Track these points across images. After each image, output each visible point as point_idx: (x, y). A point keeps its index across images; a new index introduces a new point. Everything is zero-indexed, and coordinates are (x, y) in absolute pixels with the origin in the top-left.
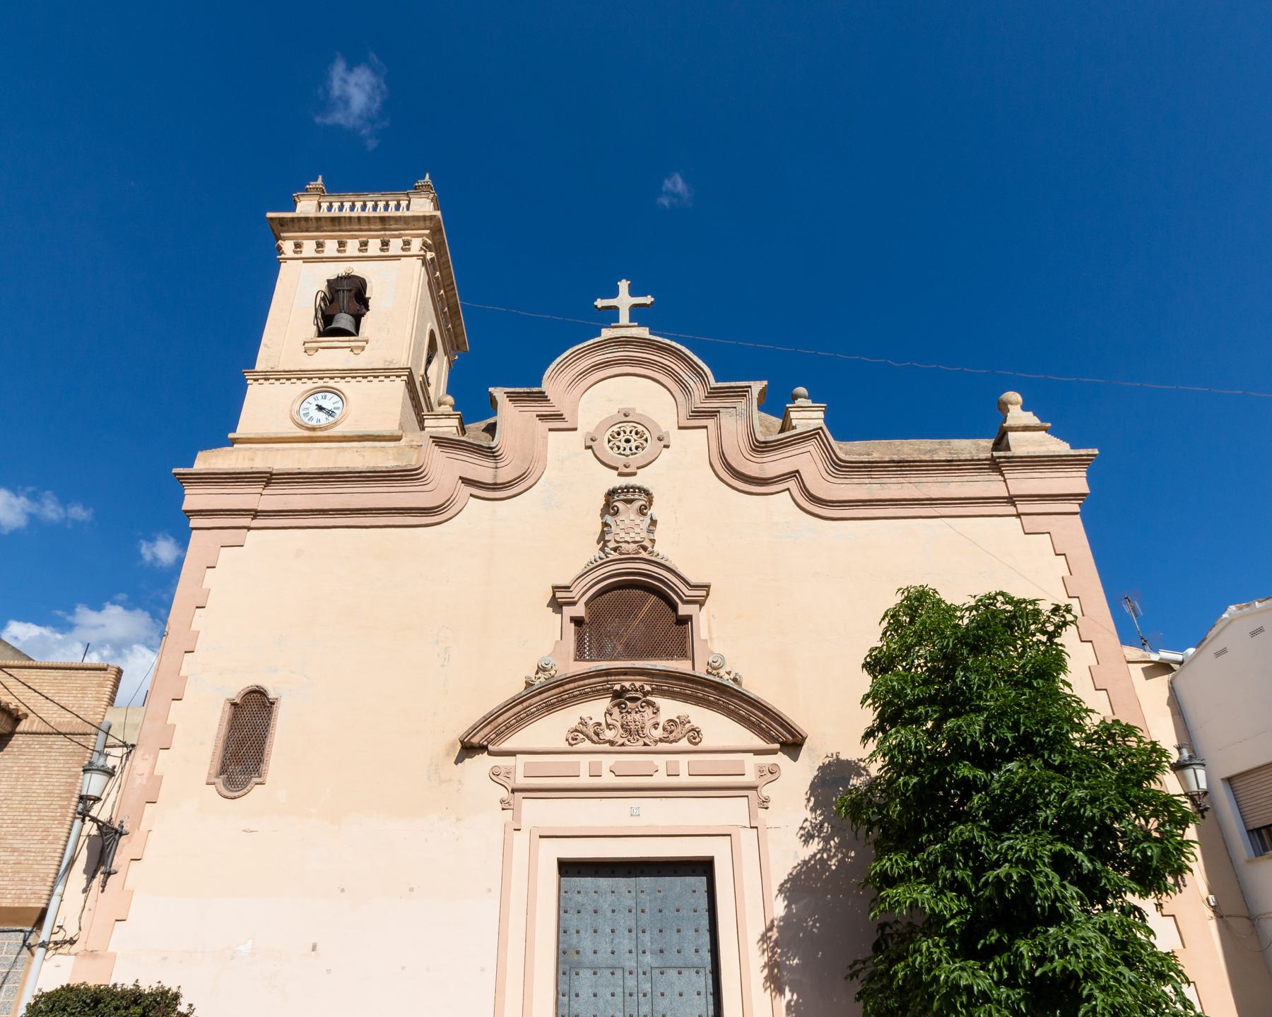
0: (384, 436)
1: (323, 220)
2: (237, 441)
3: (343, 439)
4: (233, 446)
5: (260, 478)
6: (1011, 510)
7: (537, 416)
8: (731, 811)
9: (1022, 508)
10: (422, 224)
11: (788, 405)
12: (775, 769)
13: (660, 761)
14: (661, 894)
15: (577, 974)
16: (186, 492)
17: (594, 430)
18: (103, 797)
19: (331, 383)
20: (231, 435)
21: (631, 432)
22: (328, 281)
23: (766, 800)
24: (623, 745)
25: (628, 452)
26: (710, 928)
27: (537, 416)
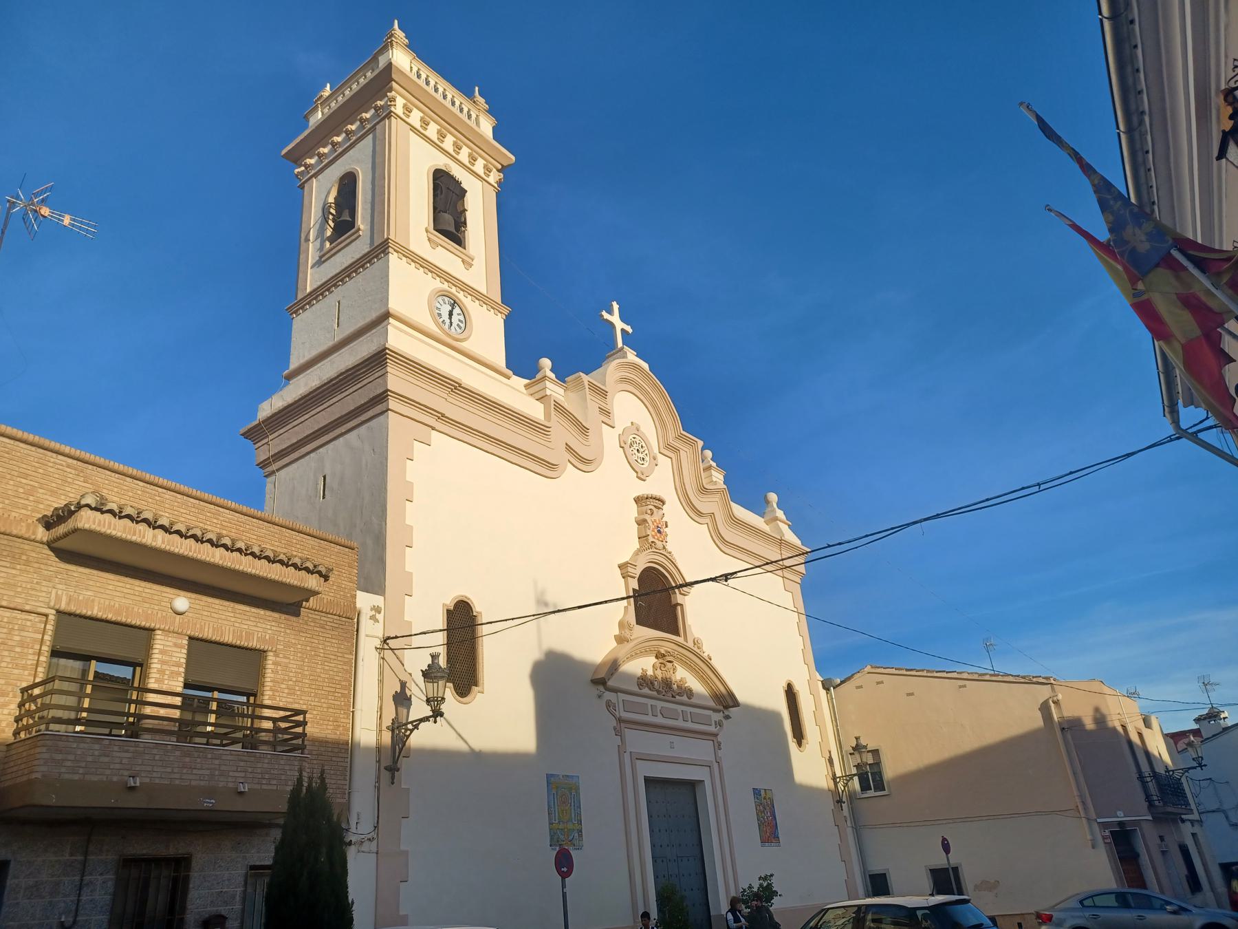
7: (599, 408)
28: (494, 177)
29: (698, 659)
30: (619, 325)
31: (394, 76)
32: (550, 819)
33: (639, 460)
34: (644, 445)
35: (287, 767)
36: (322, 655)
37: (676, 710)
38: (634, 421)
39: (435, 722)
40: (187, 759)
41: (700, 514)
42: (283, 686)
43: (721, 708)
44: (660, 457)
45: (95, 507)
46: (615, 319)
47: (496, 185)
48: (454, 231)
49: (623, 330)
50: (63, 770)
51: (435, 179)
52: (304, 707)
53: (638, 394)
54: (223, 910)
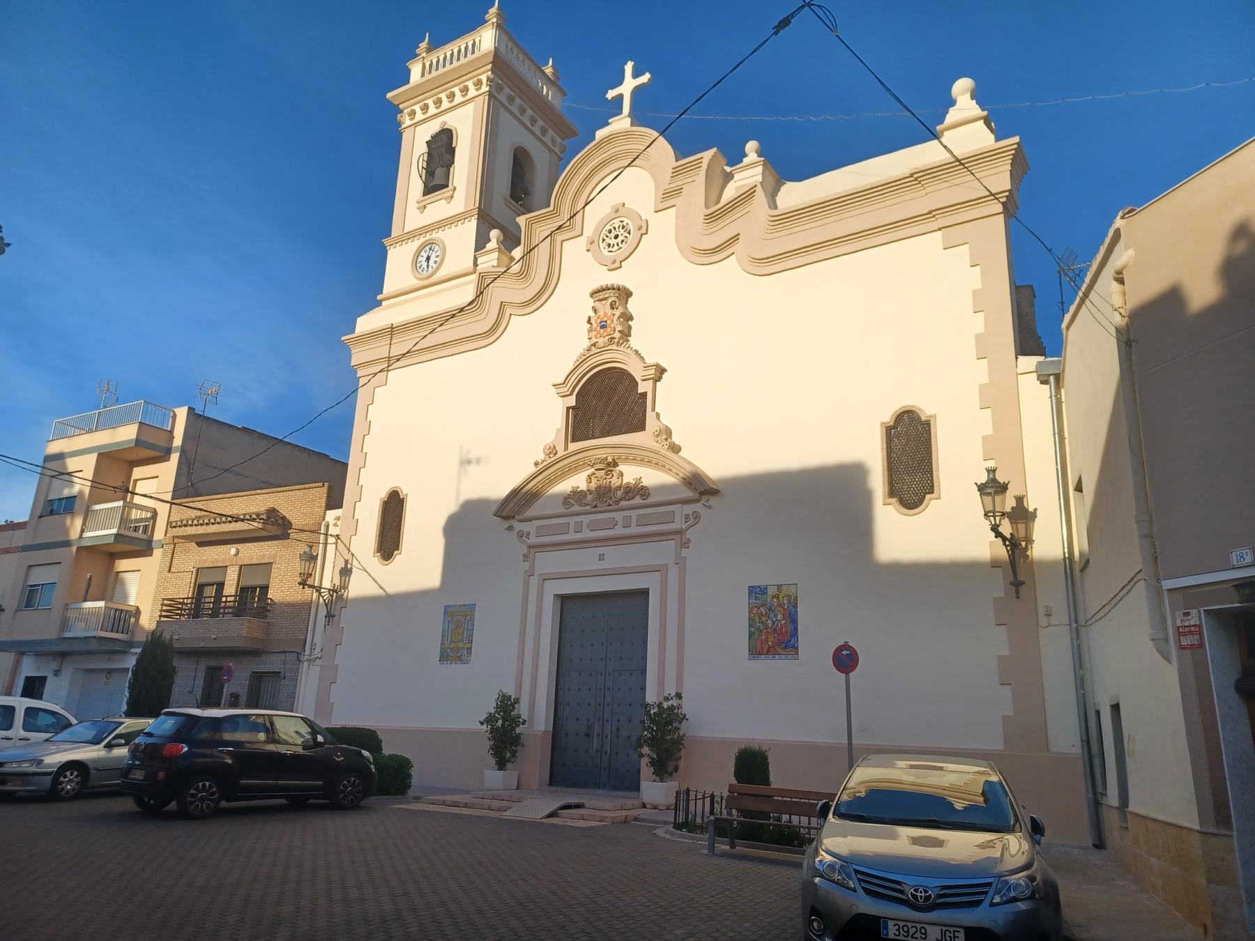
4: (381, 305)
8: (664, 552)
11: (343, 338)
12: (520, 533)
13: (618, 516)
15: (570, 675)
16: (352, 352)
17: (593, 234)
18: (348, 557)
20: (379, 297)
21: (619, 228)
22: (426, 142)
23: (689, 541)
24: (596, 506)
25: (616, 247)
29: (576, 456)
31: (396, 103)
32: (442, 641)
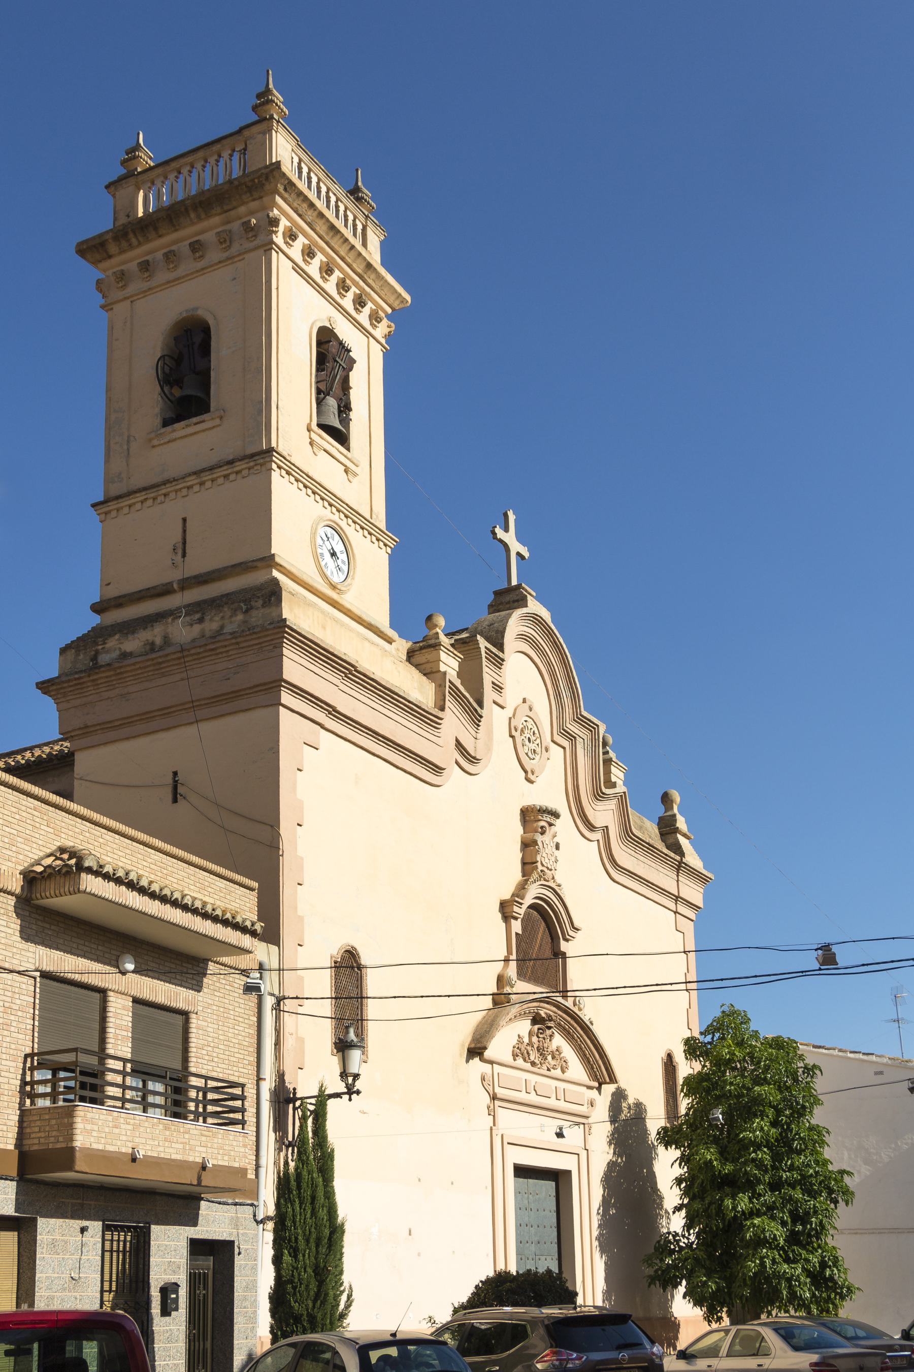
0: (386, 635)
1: (339, 236)
2: (278, 567)
3: (357, 619)
5: (637, 842)
6: (672, 905)
7: (493, 683)
9: (682, 909)
10: (391, 299)
14: (538, 1196)
19: (343, 523)
26: (275, 1285)
27: (493, 683)
28: (382, 330)
30: (516, 547)
33: (530, 754)
34: (536, 732)
35: (235, 1143)
36: (232, 1017)
37: (550, 1086)
38: (527, 697)
39: (350, 1100)
40: (167, 1133)
41: (591, 827)
42: (204, 1052)
43: (596, 1084)
44: (553, 747)
45: (96, 871)
46: (510, 538)
47: (383, 341)
48: (340, 427)
49: (506, 530)
50: (92, 1140)
51: (319, 343)
52: (241, 1080)
53: (551, 692)
54: (173, 1279)
